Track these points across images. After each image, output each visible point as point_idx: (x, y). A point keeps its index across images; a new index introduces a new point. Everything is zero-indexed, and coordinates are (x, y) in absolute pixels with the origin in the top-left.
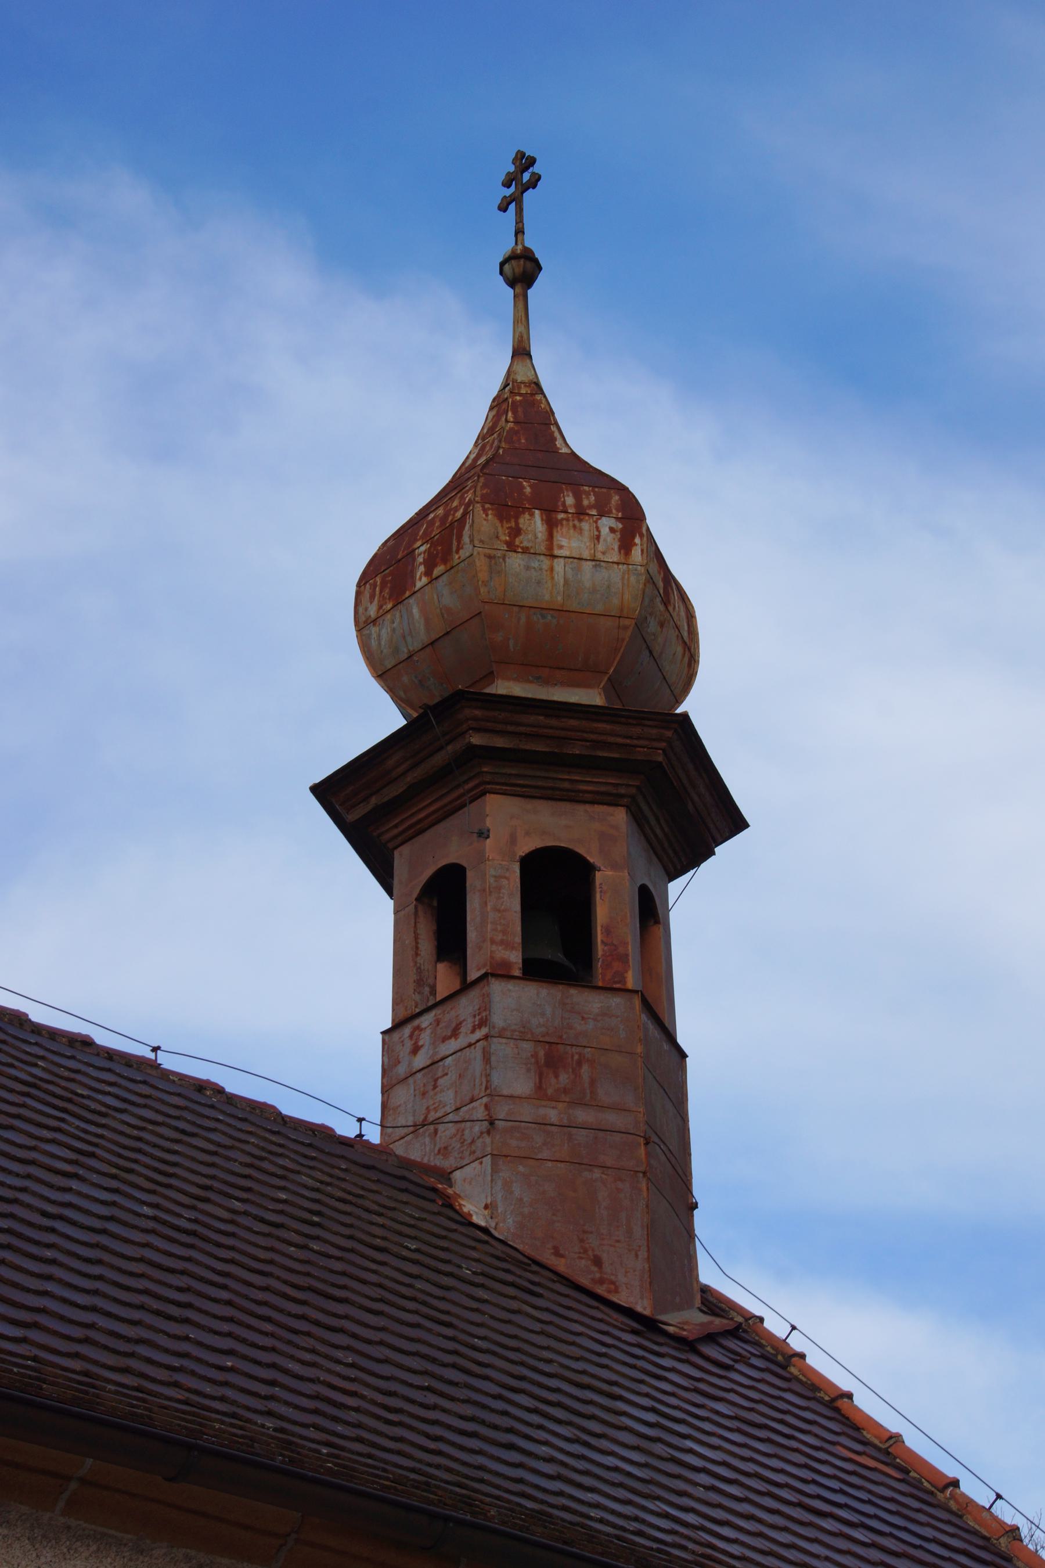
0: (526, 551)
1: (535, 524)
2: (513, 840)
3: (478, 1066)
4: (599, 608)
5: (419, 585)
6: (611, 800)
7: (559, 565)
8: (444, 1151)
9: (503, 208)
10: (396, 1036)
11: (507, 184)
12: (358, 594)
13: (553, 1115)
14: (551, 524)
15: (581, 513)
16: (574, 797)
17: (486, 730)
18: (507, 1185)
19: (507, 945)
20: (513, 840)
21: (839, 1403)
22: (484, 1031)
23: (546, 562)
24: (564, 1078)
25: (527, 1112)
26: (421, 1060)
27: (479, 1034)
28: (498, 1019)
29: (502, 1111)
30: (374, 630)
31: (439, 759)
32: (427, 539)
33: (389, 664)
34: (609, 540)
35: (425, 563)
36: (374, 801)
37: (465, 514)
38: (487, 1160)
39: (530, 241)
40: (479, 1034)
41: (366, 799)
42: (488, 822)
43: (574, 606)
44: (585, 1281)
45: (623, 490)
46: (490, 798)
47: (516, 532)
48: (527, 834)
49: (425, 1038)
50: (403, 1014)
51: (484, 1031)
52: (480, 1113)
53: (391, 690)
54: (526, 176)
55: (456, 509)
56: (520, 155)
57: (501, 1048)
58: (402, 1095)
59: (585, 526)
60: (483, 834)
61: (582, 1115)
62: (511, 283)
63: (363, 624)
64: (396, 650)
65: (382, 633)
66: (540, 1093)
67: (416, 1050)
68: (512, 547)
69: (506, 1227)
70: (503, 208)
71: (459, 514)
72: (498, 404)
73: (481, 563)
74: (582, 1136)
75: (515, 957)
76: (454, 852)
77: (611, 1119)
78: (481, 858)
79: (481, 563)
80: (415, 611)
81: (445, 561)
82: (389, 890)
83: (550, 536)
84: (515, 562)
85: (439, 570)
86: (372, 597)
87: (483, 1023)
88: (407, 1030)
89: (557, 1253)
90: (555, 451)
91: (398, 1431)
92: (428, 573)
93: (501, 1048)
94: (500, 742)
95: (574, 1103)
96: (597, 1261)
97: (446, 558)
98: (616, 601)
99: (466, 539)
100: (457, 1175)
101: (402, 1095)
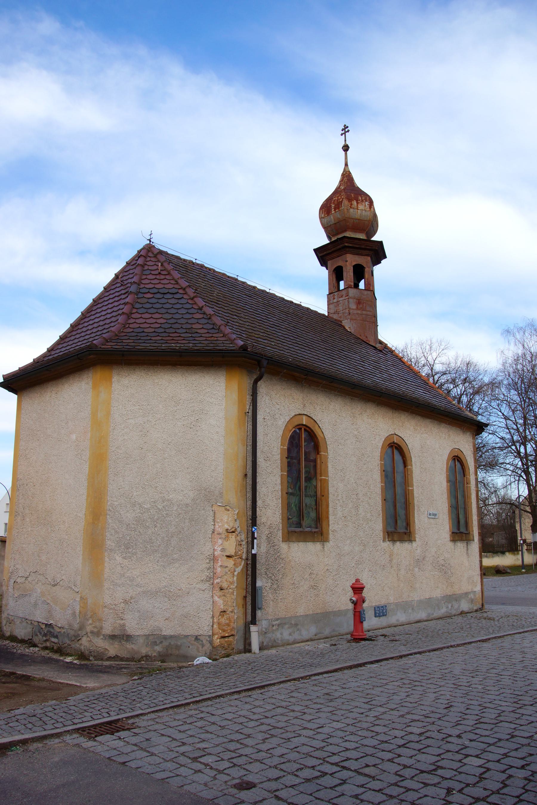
0: (353, 208)
1: (355, 203)
2: (352, 262)
3: (347, 303)
4: (366, 219)
5: (333, 212)
6: (368, 255)
7: (359, 211)
8: (340, 317)
9: (342, 135)
10: (330, 296)
11: (342, 130)
12: (320, 212)
13: (359, 312)
14: (357, 203)
15: (362, 201)
16: (362, 255)
17: (349, 243)
18: (352, 324)
19: (351, 282)
20: (352, 262)
21: (402, 359)
22: (348, 297)
23: (356, 210)
24: (361, 306)
25: (355, 312)
26: (335, 301)
27: (347, 298)
28: (350, 295)
29: (351, 312)
30: (323, 220)
31: (338, 247)
32: (334, 203)
33: (326, 226)
34: (367, 206)
35: (334, 208)
36: (325, 253)
37: (342, 200)
38: (349, 320)
39: (347, 143)
40: (347, 298)
41: (324, 252)
42: (347, 259)
43: (361, 219)
44: (365, 340)
45: (369, 196)
46: (347, 254)
47: (351, 204)
48: (354, 261)
49: (336, 297)
50: (331, 292)
51: (348, 297)
52: (347, 312)
53: (326, 231)
54: (346, 130)
55: (340, 199)
56: (345, 125)
57: (351, 300)
58: (331, 306)
59: (363, 203)
60: (347, 261)
61: (364, 312)
62: (344, 151)
63: (321, 218)
64: (328, 224)
65: (325, 220)
66: (357, 309)
67: (334, 299)
68: (351, 207)
69: (352, 331)
70: (342, 135)
71: (341, 200)
72: (343, 175)
73: (346, 210)
74: (364, 316)
75: (352, 284)
76: (340, 264)
77: (369, 313)
78: (346, 265)
79: (346, 210)
80: (332, 217)
81: (338, 209)
82: (327, 269)
83: (357, 206)
84: (351, 210)
85: (337, 210)
86: (323, 213)
87: (347, 296)
88: (332, 295)
89: (360, 336)
90: (355, 186)
91: (233, 297)
92: (335, 210)
93: (351, 300)
94: (350, 245)
95: (363, 310)
96: (367, 337)
97: (338, 208)
98: (368, 218)
99: (343, 205)
100: (343, 322)
101: (331, 306)
